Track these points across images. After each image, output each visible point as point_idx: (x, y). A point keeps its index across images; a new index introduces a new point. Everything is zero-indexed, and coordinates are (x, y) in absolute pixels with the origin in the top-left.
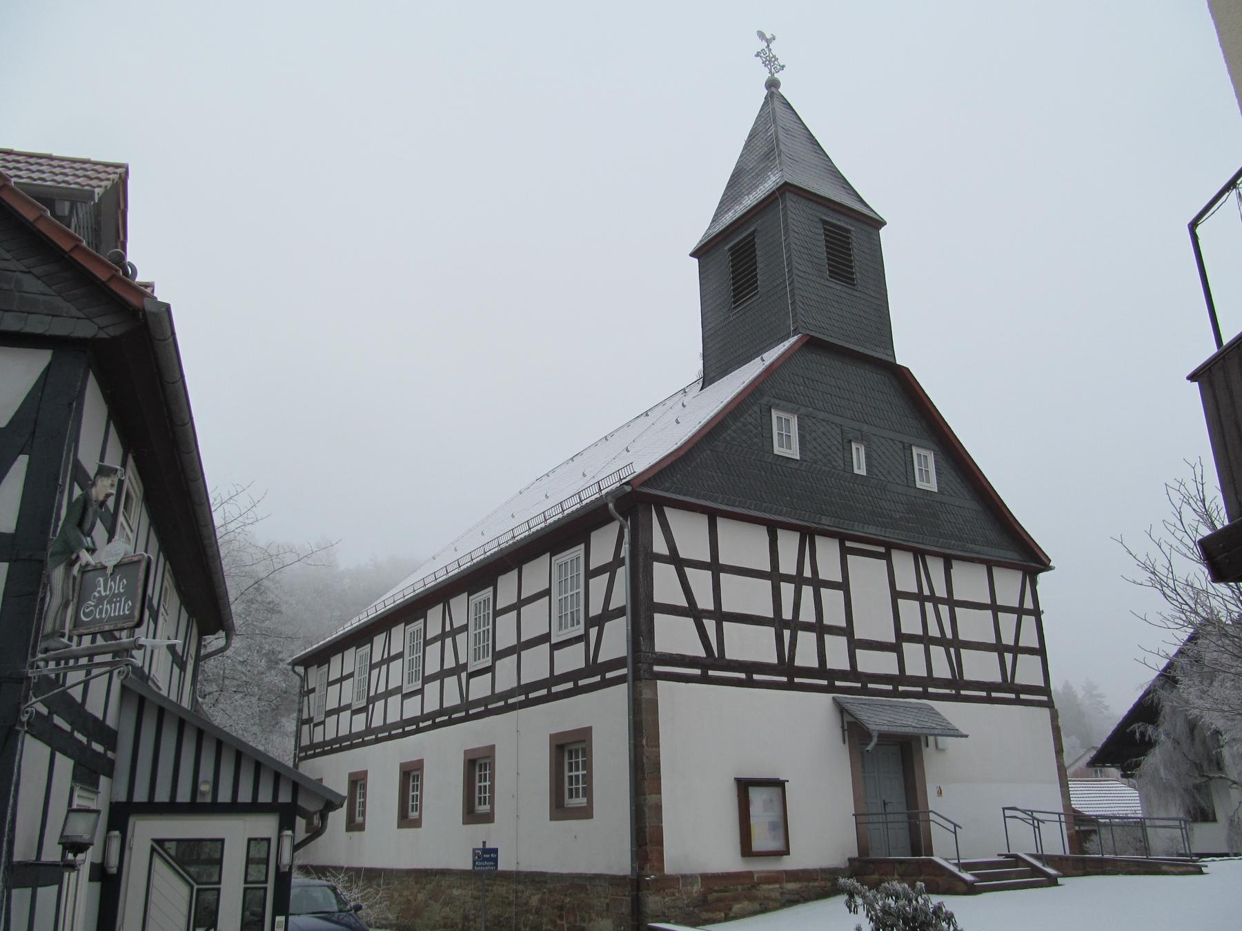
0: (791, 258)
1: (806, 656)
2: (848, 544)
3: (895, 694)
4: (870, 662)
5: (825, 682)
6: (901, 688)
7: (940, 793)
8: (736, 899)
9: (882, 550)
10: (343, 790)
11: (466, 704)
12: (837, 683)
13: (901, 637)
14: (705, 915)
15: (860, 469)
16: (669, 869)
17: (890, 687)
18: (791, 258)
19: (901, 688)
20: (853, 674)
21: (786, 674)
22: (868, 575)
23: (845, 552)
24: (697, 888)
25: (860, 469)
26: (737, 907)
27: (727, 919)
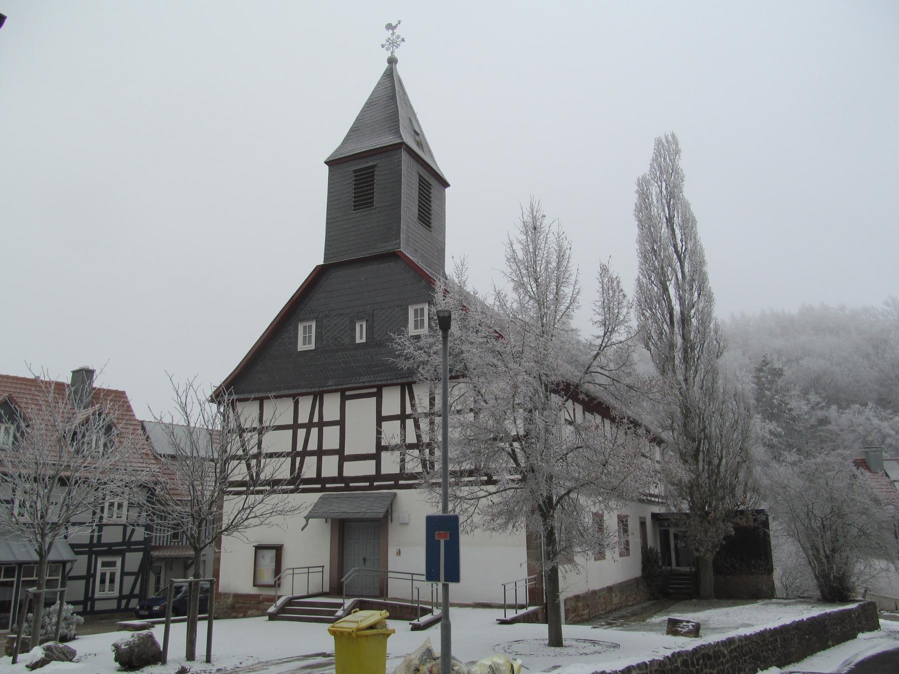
0: (382, 182)
1: (309, 469)
2: (347, 393)
3: (371, 487)
4: (352, 469)
5: (319, 486)
6: (375, 484)
7: (399, 553)
8: (249, 608)
9: (375, 390)
10: (36, 558)
11: (341, 478)
12: (327, 486)
13: (380, 448)
14: (233, 614)
15: (360, 337)
16: (221, 590)
17: (368, 484)
18: (382, 182)
19: (375, 484)
20: (341, 478)
21: (296, 483)
22: (361, 412)
23: (344, 399)
24: (230, 601)
25: (360, 337)
26: (250, 612)
27: (245, 616)
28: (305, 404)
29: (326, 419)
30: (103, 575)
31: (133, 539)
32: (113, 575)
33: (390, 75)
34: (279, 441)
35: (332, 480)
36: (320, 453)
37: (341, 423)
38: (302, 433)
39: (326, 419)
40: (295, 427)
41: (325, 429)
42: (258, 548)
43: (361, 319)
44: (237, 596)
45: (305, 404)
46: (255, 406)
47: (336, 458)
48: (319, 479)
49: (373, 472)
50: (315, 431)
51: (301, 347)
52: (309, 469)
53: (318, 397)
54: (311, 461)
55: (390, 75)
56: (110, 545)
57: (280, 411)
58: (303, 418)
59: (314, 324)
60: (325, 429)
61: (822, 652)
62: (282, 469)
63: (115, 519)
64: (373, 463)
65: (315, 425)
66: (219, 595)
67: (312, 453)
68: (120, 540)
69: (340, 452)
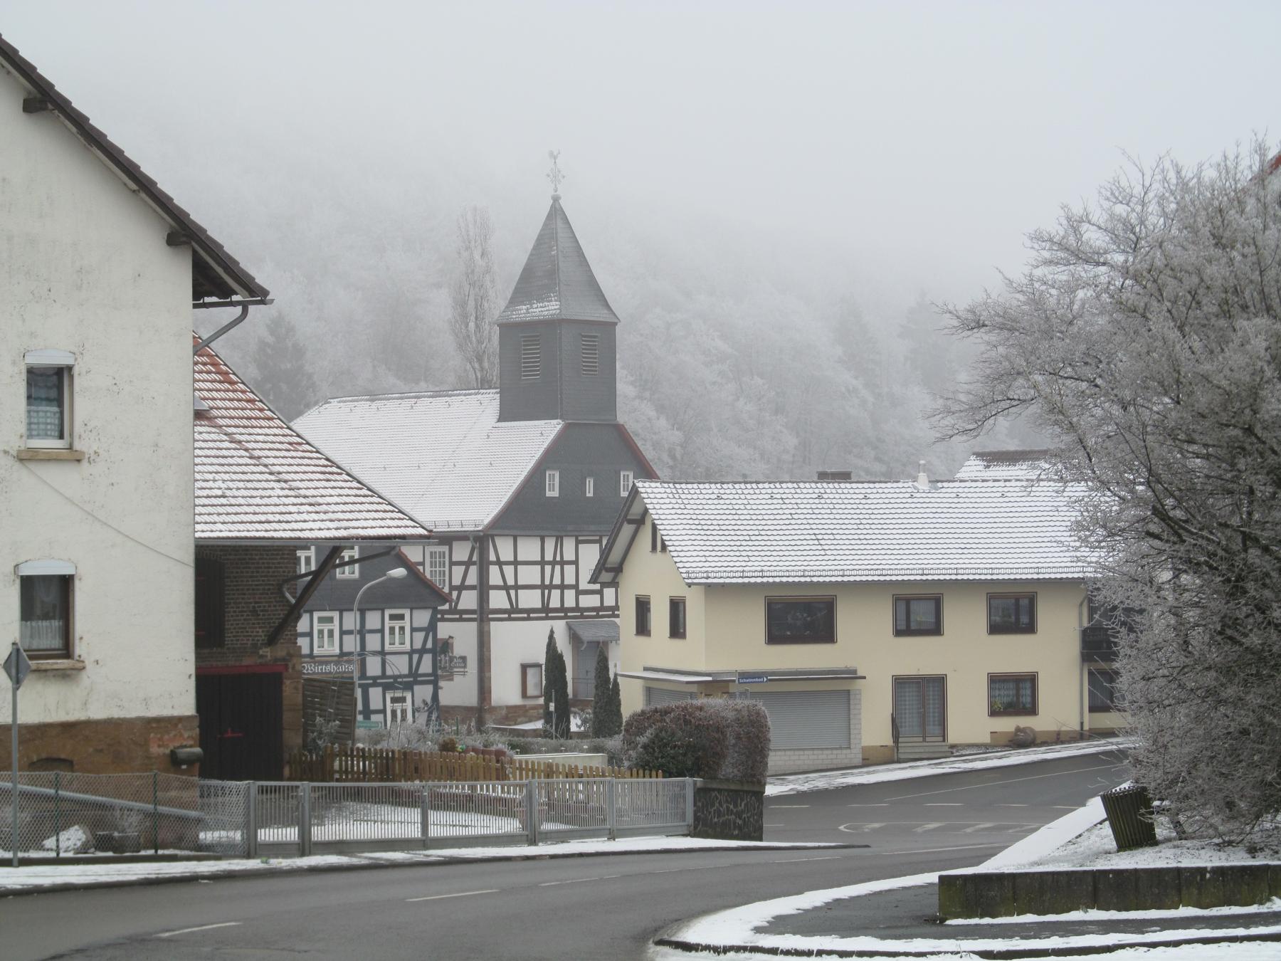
1: (555, 603)
3: (598, 616)
16: (493, 704)
21: (545, 612)
23: (578, 542)
24: (504, 712)
28: (550, 544)
29: (566, 558)
30: (394, 713)
31: (420, 671)
32: (404, 712)
33: (556, 199)
34: (530, 575)
35: (572, 610)
36: (562, 587)
37: (575, 563)
38: (548, 568)
39: (566, 558)
40: (542, 563)
41: (519, 559)
42: (524, 668)
43: (590, 476)
44: (509, 708)
45: (550, 544)
46: (510, 541)
47: (573, 591)
48: (562, 609)
49: (492, 583)
50: (558, 568)
51: (549, 494)
52: (555, 603)
53: (559, 540)
54: (556, 594)
55: (556, 199)
56: (395, 677)
57: (529, 549)
58: (549, 557)
59: (557, 475)
60: (519, 559)
61: (191, 668)
62: (530, 599)
63: (397, 647)
64: (598, 596)
65: (558, 563)
66: (493, 709)
67: (556, 587)
68: (406, 671)
69: (575, 587)
